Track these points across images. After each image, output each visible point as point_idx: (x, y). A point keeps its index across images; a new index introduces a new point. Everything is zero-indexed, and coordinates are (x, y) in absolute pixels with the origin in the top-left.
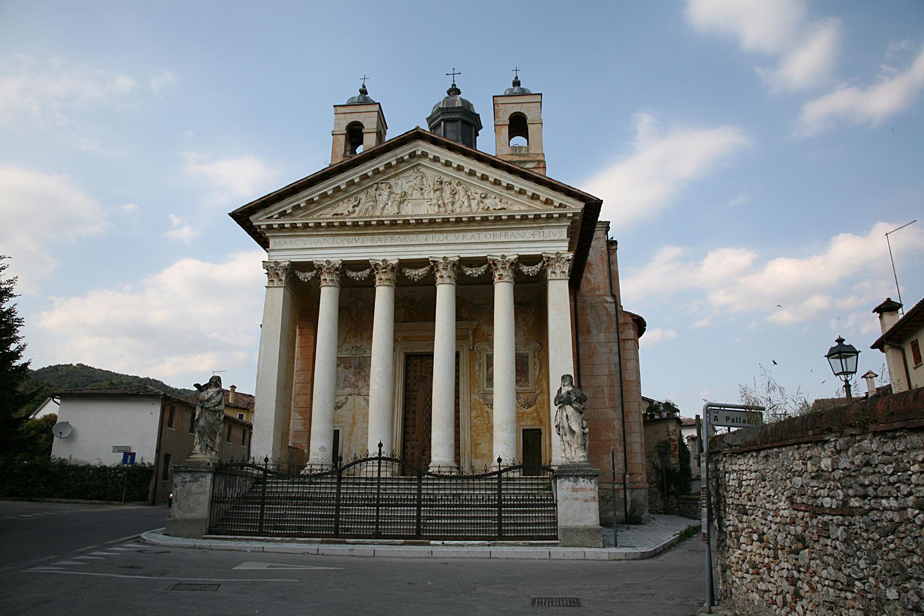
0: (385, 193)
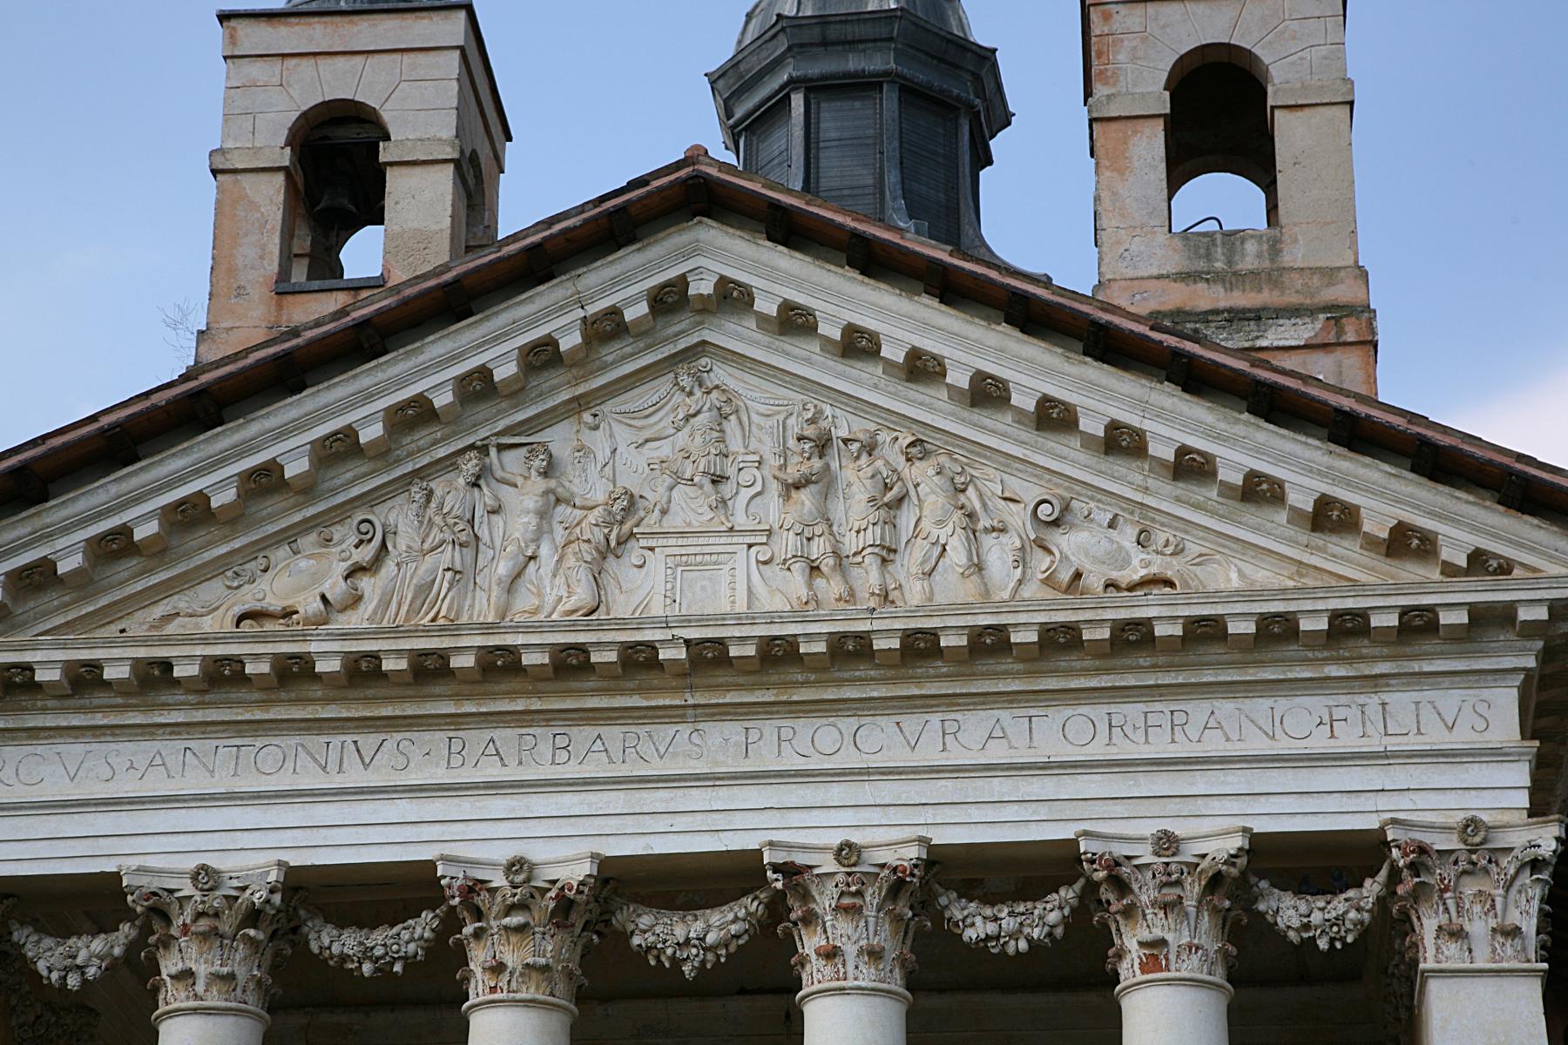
0: (523, 501)
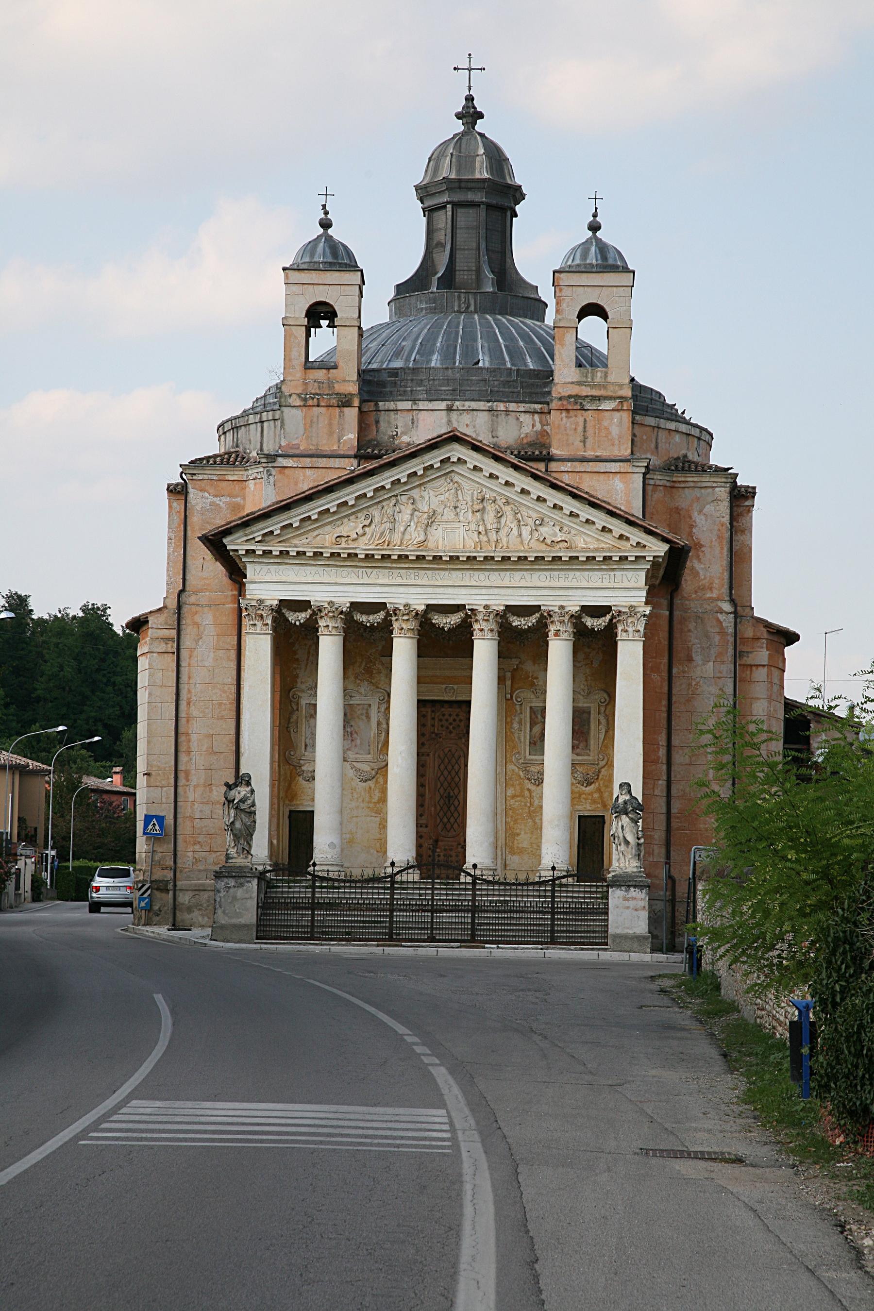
0: (407, 510)
